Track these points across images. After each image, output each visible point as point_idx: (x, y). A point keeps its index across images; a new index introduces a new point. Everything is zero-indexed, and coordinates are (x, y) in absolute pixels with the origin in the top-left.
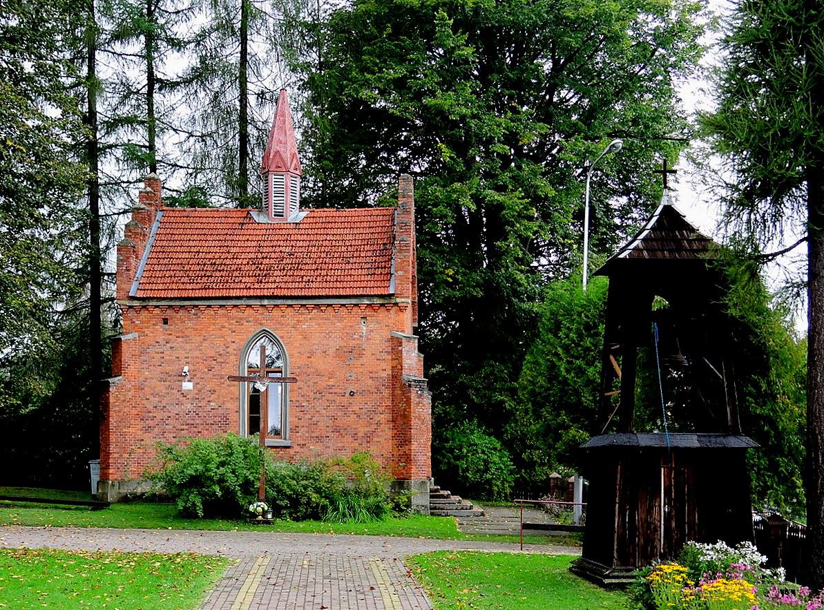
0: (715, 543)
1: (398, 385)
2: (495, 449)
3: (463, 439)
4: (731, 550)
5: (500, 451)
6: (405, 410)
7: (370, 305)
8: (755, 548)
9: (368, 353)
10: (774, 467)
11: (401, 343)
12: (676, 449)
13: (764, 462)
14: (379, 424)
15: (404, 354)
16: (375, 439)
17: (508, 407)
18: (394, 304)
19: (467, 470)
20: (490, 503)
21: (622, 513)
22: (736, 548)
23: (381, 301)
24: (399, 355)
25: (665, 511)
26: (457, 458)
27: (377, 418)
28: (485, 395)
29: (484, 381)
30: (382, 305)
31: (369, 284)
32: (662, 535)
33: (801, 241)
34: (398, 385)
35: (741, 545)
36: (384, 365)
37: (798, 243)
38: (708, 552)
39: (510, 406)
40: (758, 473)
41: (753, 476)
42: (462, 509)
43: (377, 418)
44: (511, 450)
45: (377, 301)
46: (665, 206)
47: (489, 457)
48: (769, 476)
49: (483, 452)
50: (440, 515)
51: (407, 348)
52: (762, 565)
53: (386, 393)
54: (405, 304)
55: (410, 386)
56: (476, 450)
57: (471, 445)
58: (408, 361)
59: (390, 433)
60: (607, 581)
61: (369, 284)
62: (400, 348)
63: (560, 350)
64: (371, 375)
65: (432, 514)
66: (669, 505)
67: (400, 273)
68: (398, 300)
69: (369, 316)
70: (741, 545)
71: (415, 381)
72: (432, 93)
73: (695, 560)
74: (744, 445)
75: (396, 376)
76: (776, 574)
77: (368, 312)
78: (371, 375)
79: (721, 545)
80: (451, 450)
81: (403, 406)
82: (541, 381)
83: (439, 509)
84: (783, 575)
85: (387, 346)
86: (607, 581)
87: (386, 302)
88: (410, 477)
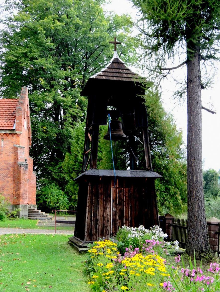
0: (138, 226)
1: (17, 167)
2: (62, 195)
3: (49, 191)
4: (147, 231)
5: (63, 195)
6: (18, 176)
7: (5, 134)
8: (161, 229)
9: (4, 153)
10: (167, 189)
11: (17, 149)
12: (118, 178)
13: (163, 188)
14: (8, 182)
15: (19, 154)
16: (6, 188)
17: (67, 179)
18: (15, 133)
19: (50, 202)
20: (59, 215)
21: (90, 212)
22: (150, 230)
23: (10, 132)
24: (17, 154)
25: (113, 211)
26: (46, 198)
27: (7, 180)
28: (58, 175)
29: (58, 170)
30: (10, 134)
31: (5, 125)
32: (112, 224)
33: (183, 64)
34: (16, 166)
35: (153, 227)
36: (11, 158)
37: (180, 66)
38: (133, 232)
39: (67, 179)
40: (160, 194)
41: (158, 194)
42: (43, 217)
43: (7, 180)
44: (68, 195)
45: (8, 132)
46: (115, 59)
47: (59, 198)
48: (165, 195)
49: (57, 196)
50: (33, 219)
51: (20, 151)
52: (165, 239)
53: (11, 169)
54: (20, 134)
55: (20, 166)
56: (54, 195)
57: (52, 193)
58: (21, 157)
59: (12, 186)
60: (80, 249)
61: (5, 125)
62: (17, 151)
63: (79, 149)
64: (5, 162)
65: (29, 219)
66: (116, 207)
67: (18, 121)
68: (17, 132)
69: (5, 138)
70: (153, 227)
71: (23, 164)
72: (37, 59)
73: (125, 237)
74: (154, 176)
75: (15, 162)
76: (173, 245)
77: (4, 137)
78: (5, 162)
79: (142, 227)
80: (45, 196)
81: (17, 174)
82: (71, 162)
83: (33, 217)
84: (177, 245)
85: (12, 151)
86: (80, 249)
87: (12, 132)
88: (20, 203)
